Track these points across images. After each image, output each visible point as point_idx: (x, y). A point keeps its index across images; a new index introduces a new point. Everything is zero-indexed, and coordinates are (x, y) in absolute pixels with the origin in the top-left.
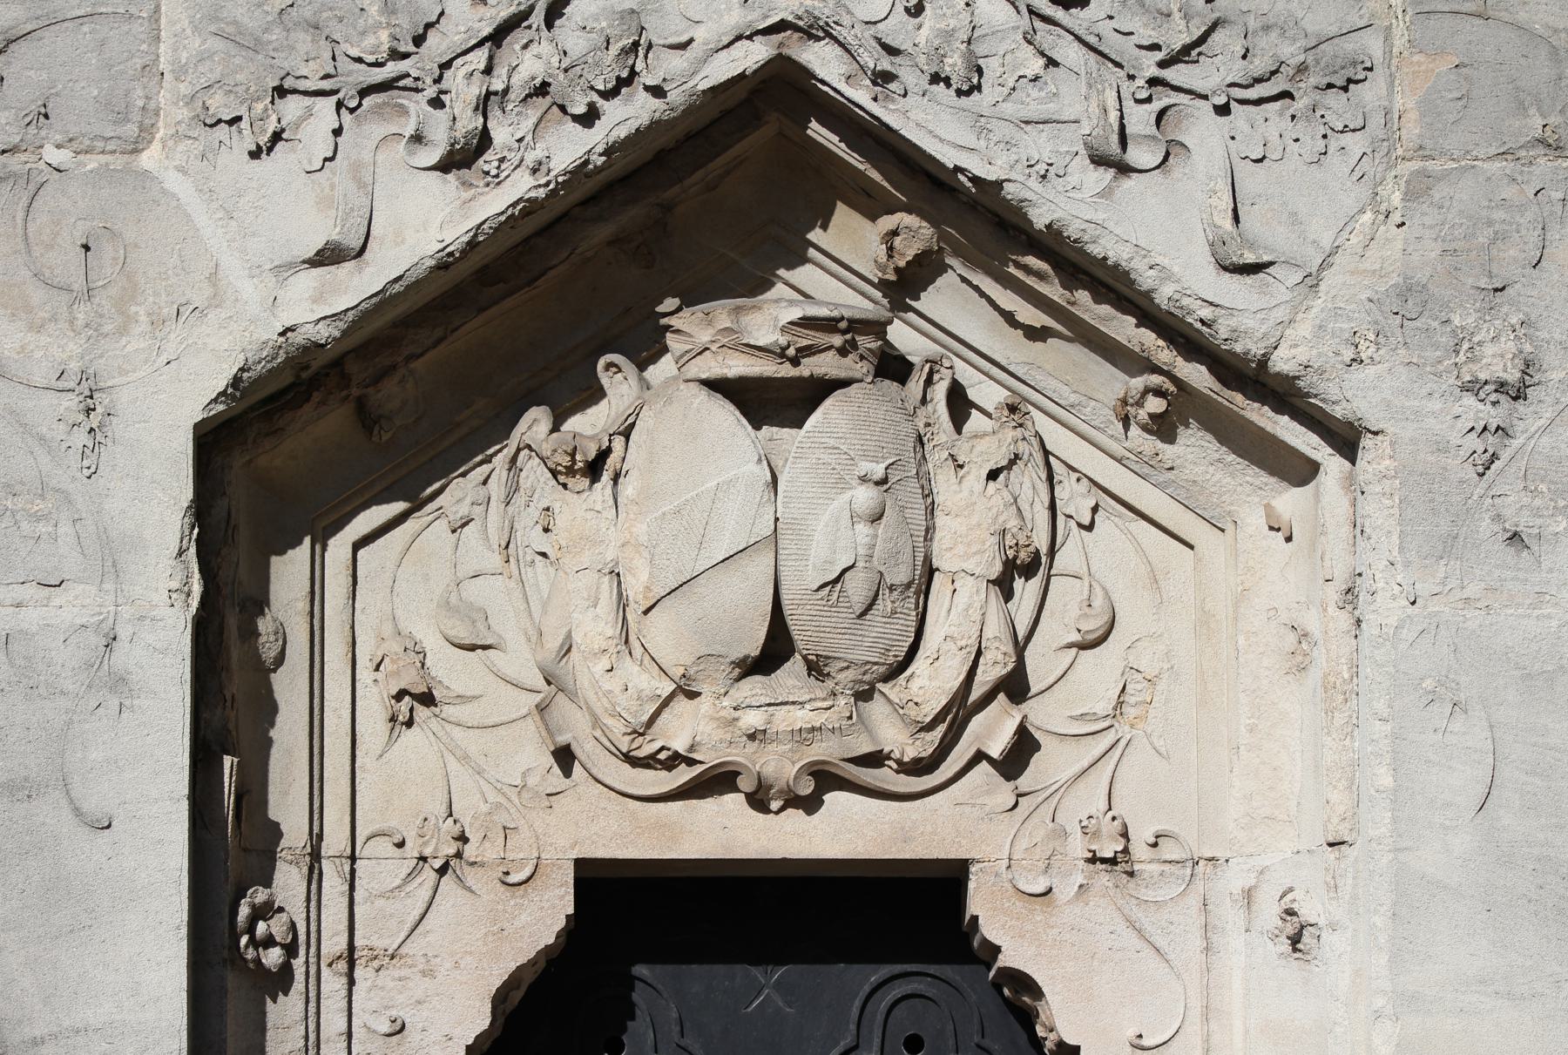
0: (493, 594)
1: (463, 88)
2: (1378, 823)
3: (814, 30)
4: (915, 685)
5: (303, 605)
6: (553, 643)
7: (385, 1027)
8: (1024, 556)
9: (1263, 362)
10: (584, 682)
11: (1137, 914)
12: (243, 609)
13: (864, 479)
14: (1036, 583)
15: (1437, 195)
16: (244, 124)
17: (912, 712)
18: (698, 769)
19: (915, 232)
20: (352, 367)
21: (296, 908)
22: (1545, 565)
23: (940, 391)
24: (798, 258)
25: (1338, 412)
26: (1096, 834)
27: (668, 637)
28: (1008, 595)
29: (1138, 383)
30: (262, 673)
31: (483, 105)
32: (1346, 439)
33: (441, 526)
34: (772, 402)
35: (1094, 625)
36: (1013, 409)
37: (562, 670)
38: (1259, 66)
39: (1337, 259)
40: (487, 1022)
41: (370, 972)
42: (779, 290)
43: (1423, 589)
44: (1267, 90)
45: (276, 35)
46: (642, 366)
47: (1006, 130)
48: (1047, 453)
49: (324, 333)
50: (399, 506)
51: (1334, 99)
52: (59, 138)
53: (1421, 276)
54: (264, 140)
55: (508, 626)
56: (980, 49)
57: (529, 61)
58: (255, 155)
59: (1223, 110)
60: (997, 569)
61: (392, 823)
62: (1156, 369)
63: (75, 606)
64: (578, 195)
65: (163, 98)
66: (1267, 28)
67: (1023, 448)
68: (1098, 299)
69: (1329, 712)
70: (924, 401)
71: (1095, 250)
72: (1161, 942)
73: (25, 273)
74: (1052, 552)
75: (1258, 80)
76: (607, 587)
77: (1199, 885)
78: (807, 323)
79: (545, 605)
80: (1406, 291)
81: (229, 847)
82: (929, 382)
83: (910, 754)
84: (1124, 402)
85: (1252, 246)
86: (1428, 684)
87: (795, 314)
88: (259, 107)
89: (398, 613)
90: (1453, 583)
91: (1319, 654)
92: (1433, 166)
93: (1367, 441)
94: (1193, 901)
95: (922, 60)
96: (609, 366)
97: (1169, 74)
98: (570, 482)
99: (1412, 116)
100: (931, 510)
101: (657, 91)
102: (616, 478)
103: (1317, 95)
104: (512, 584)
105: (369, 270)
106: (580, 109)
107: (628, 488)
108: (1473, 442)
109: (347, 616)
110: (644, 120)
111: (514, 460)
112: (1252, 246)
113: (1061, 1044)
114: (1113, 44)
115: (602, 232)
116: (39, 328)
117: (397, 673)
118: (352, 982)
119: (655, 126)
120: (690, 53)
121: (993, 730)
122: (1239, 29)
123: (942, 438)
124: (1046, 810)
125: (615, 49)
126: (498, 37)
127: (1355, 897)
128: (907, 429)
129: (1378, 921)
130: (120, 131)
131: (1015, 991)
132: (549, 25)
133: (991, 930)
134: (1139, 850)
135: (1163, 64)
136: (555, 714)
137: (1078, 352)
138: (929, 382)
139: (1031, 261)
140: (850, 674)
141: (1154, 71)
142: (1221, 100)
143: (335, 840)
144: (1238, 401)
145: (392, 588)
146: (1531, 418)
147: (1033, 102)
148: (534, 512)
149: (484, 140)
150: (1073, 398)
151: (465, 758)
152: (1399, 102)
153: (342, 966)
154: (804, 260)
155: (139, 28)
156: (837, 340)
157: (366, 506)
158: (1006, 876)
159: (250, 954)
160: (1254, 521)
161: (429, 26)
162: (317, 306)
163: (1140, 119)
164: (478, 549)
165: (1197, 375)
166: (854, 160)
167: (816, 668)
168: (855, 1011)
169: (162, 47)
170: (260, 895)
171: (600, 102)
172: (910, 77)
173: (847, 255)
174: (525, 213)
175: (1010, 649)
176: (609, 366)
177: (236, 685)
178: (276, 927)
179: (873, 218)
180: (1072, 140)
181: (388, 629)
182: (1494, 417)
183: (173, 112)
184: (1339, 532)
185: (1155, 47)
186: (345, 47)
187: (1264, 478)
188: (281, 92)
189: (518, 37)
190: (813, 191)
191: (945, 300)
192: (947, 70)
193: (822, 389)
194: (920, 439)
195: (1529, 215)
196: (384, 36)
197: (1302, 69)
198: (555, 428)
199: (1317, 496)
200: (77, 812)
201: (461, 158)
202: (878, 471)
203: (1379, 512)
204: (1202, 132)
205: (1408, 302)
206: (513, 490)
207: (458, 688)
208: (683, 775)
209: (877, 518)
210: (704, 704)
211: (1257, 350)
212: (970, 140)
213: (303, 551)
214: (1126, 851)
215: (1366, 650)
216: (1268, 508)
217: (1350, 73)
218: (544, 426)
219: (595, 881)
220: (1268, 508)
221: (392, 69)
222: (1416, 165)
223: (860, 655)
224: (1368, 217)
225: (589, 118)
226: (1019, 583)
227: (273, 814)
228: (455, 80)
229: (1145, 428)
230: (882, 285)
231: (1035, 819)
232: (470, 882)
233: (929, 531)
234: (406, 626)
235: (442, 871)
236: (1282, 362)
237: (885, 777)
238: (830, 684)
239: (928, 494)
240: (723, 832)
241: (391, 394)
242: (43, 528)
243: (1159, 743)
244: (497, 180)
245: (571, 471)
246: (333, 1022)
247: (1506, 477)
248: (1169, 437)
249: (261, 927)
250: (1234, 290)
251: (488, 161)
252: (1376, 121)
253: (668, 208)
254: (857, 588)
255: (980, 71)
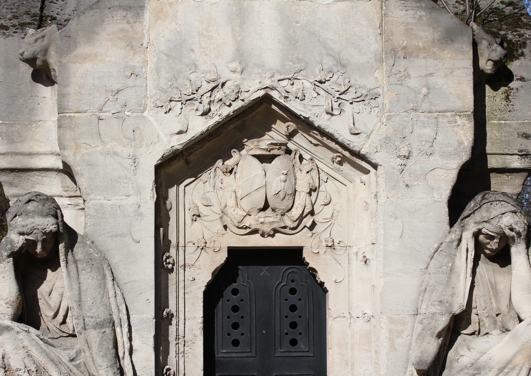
0: (212, 196)
1: (206, 100)
2: (381, 240)
3: (273, 88)
4: (293, 213)
5: (175, 198)
6: (223, 205)
7: (191, 279)
8: (314, 188)
9: (359, 152)
10: (229, 213)
11: (336, 256)
12: (164, 199)
13: (283, 174)
14: (316, 193)
15: (392, 119)
16: (164, 107)
17: (292, 218)
18: (251, 229)
19: (293, 126)
20: (184, 153)
21: (174, 257)
22: (413, 190)
23: (297, 156)
24: (270, 130)
25: (373, 161)
26: (328, 241)
27: (246, 204)
28: (311, 195)
29: (336, 155)
30: (167, 211)
31: (209, 103)
32: (375, 166)
33: (201, 182)
34: (265, 159)
35: (327, 201)
36: (311, 160)
37: (225, 210)
38: (358, 95)
39: (373, 132)
40: (38, 290)
41: (188, 269)
42: (266, 137)
43: (390, 195)
44: (360, 99)
45: (170, 90)
46: (240, 151)
47: (310, 107)
48: (318, 168)
49: (179, 147)
50: (193, 179)
51: (373, 101)
52: (128, 110)
53: (389, 135)
54: (167, 110)
55: (214, 202)
56: (305, 92)
57: (218, 94)
58: (166, 113)
59: (351, 103)
60: (308, 190)
61: (192, 240)
62: (339, 152)
63: (132, 200)
64: (228, 120)
65: (148, 102)
66: (360, 87)
67: (313, 167)
68: (328, 139)
69: (372, 218)
70: (294, 158)
71: (327, 130)
72: (340, 262)
73: (122, 136)
74: (319, 187)
75: (358, 98)
76: (233, 194)
77: (347, 251)
78: (272, 144)
79: (222, 198)
80: (386, 138)
81: (162, 246)
82: (295, 154)
83: (292, 226)
84: (333, 158)
85: (357, 130)
86: (390, 214)
87: (270, 142)
88: (167, 104)
89: (194, 199)
90: (395, 194)
91: (370, 207)
92: (391, 114)
93: (379, 167)
94: (346, 254)
95: (294, 94)
96: (234, 151)
97: (341, 96)
98: (226, 174)
99: (388, 104)
100: (296, 179)
101: (243, 100)
102: (235, 173)
103: (370, 100)
104: (215, 194)
105: (188, 135)
106: (228, 104)
107: (237, 175)
108: (399, 167)
109: (183, 200)
110: (240, 106)
111: (215, 170)
112: (357, 130)
113: (321, 282)
114: (330, 91)
115: (233, 126)
116: (125, 146)
117: (193, 211)
118: (185, 270)
119: (242, 107)
120: (249, 93)
121: (308, 221)
122: (354, 88)
123: (298, 165)
124: (318, 237)
125: (235, 92)
126: (212, 90)
127: (377, 254)
128: (291, 164)
129: (381, 259)
130: (140, 108)
131: (312, 271)
132: (222, 88)
133: (307, 260)
134: (336, 244)
135: (340, 95)
136: (223, 219)
137: (324, 149)
138: (295, 154)
139: (315, 132)
140: (280, 211)
141: (338, 96)
142: (351, 102)
143: (181, 243)
144: (355, 159)
145: (191, 194)
146: (410, 162)
147: (315, 102)
148: (219, 180)
149: (210, 110)
150: (323, 157)
151: (206, 227)
152: (385, 101)
153: (183, 267)
154: (271, 130)
155: (143, 88)
156: (278, 147)
157: (187, 179)
158: (310, 249)
159: (166, 266)
160: (358, 181)
161: (199, 88)
162: (178, 142)
163: (335, 105)
164: (208, 187)
165: (347, 154)
166: (281, 112)
167: (274, 210)
168: (281, 275)
169: (148, 92)
170: (167, 254)
171: (232, 102)
172: (291, 97)
173: (278, 131)
174: (218, 124)
175: (311, 206)
176: (234, 151)
177: (163, 214)
178: (170, 260)
179: (285, 123)
180: (322, 109)
181: (191, 203)
182: (403, 162)
183: (150, 105)
184: (374, 184)
185: (338, 91)
186: (183, 92)
187: (360, 173)
188: (171, 101)
189: (216, 90)
190: (273, 118)
191: (299, 138)
192: (298, 96)
193: (274, 157)
194: (293, 166)
195: (410, 123)
196: (190, 90)
197: (367, 95)
198: (223, 164)
199: (370, 176)
200: (133, 239)
201: (205, 113)
202: (286, 172)
203: (381, 181)
204: (347, 107)
205: (387, 140)
206: (215, 175)
207: (205, 214)
208: (248, 230)
209: (285, 181)
210: (252, 217)
211: (358, 150)
212: (303, 109)
213: (175, 188)
214: (333, 244)
215: (379, 207)
216: (361, 179)
217: (376, 96)
218: (221, 163)
219: (232, 251)
220: (361, 179)
221: (192, 96)
222: (388, 114)
223: (282, 208)
224: (379, 124)
225: (230, 105)
226: (313, 193)
227: (170, 238)
228: (204, 98)
229: (337, 163)
230: (286, 135)
231: (316, 239)
232: (207, 251)
233: (295, 183)
234: (195, 202)
235: (202, 249)
236: (363, 152)
237: (287, 231)
238: (276, 213)
239: (295, 176)
240: (256, 241)
241: (192, 158)
242: (126, 185)
243: (340, 224)
244: (212, 118)
245: (226, 172)
246: (181, 278)
247: (405, 174)
248: (341, 165)
249: (168, 260)
250: (354, 138)
251: (210, 114)
252: (381, 105)
253: (245, 121)
254: (281, 195)
255: (305, 96)
